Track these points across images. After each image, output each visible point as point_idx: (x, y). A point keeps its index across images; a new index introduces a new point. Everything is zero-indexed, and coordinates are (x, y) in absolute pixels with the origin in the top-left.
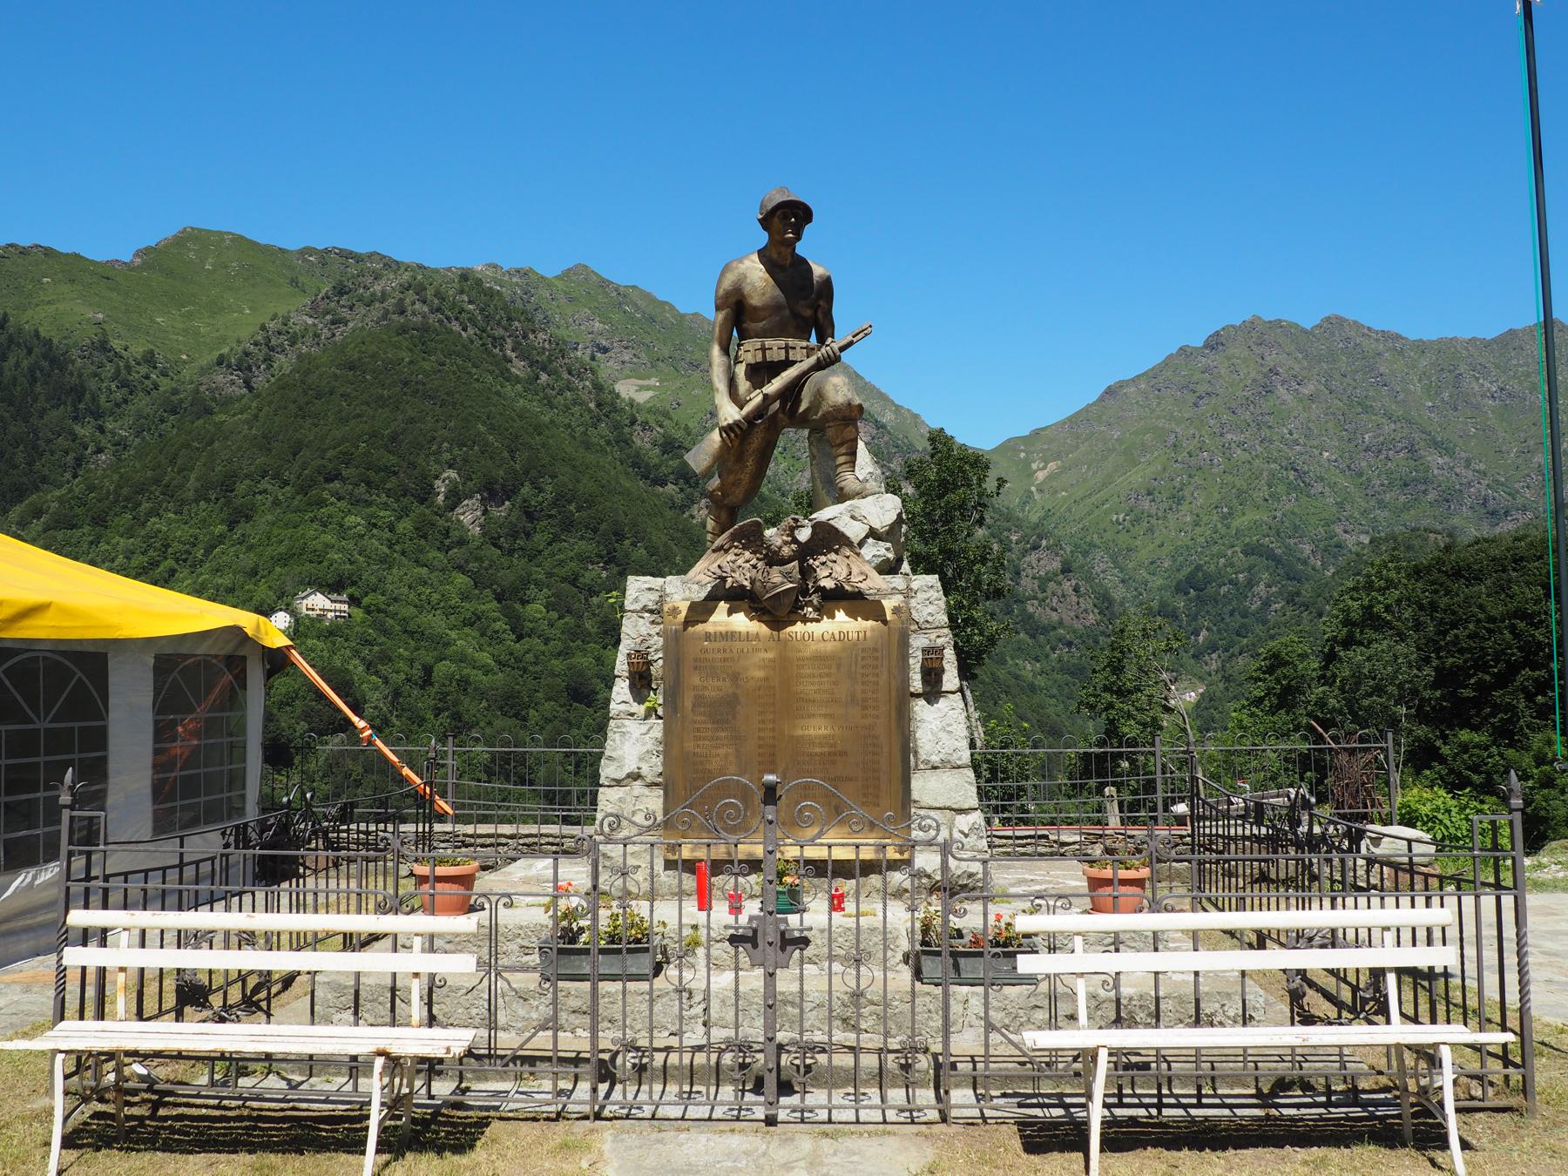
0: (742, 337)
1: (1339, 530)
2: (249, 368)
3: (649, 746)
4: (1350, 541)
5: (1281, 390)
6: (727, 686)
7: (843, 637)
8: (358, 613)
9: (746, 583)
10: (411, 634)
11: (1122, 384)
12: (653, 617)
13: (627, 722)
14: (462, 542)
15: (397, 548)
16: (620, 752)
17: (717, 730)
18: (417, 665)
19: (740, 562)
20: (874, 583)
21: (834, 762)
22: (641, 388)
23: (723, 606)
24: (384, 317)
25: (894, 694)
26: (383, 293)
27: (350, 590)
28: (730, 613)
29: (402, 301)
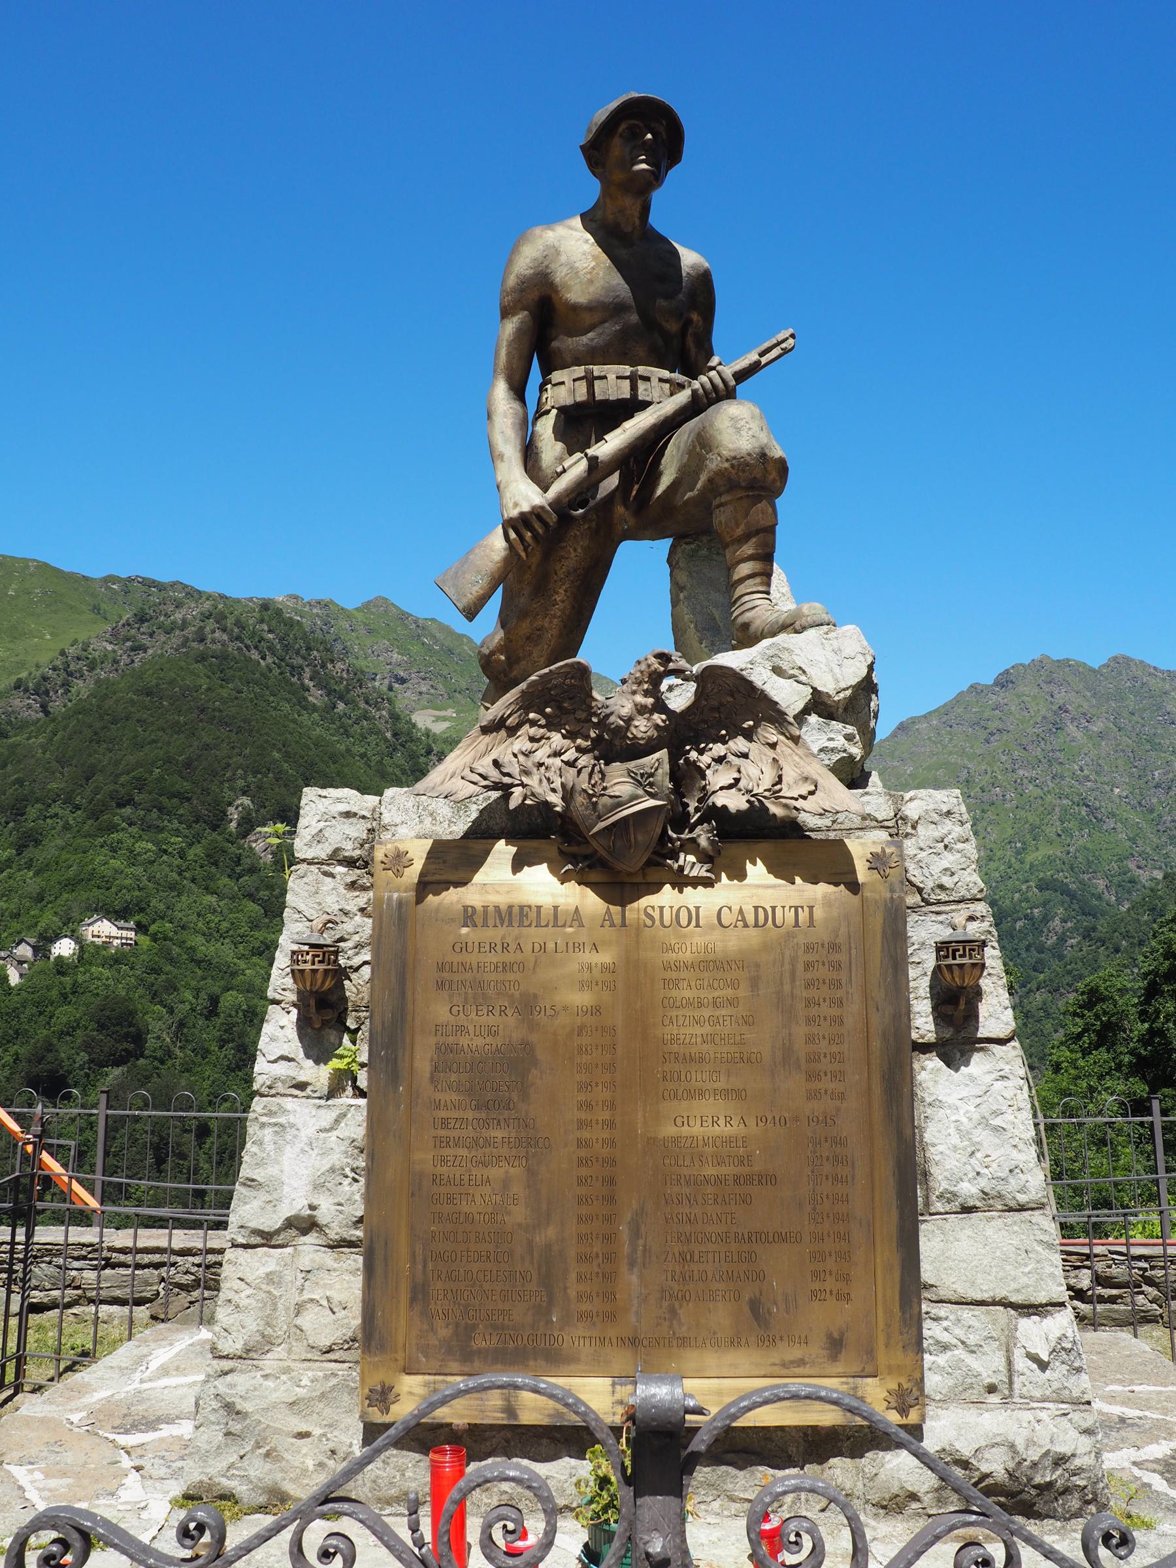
0: (547, 370)
1: (1132, 865)
2: (47, 693)
3: (337, 1158)
4: (1144, 876)
5: (1071, 728)
6: (509, 1025)
7: (764, 918)
8: (145, 941)
9: (555, 799)
10: (198, 963)
11: (914, 721)
12: (353, 875)
13: (289, 1103)
14: (253, 870)
15: (187, 875)
16: (272, 1170)
17: (486, 1123)
18: (203, 995)
19: (541, 754)
20: (824, 804)
21: (746, 1200)
22: (438, 719)
23: (503, 851)
24: (184, 645)
25: (876, 1044)
26: (184, 620)
27: (137, 918)
28: (518, 864)
29: (202, 628)
